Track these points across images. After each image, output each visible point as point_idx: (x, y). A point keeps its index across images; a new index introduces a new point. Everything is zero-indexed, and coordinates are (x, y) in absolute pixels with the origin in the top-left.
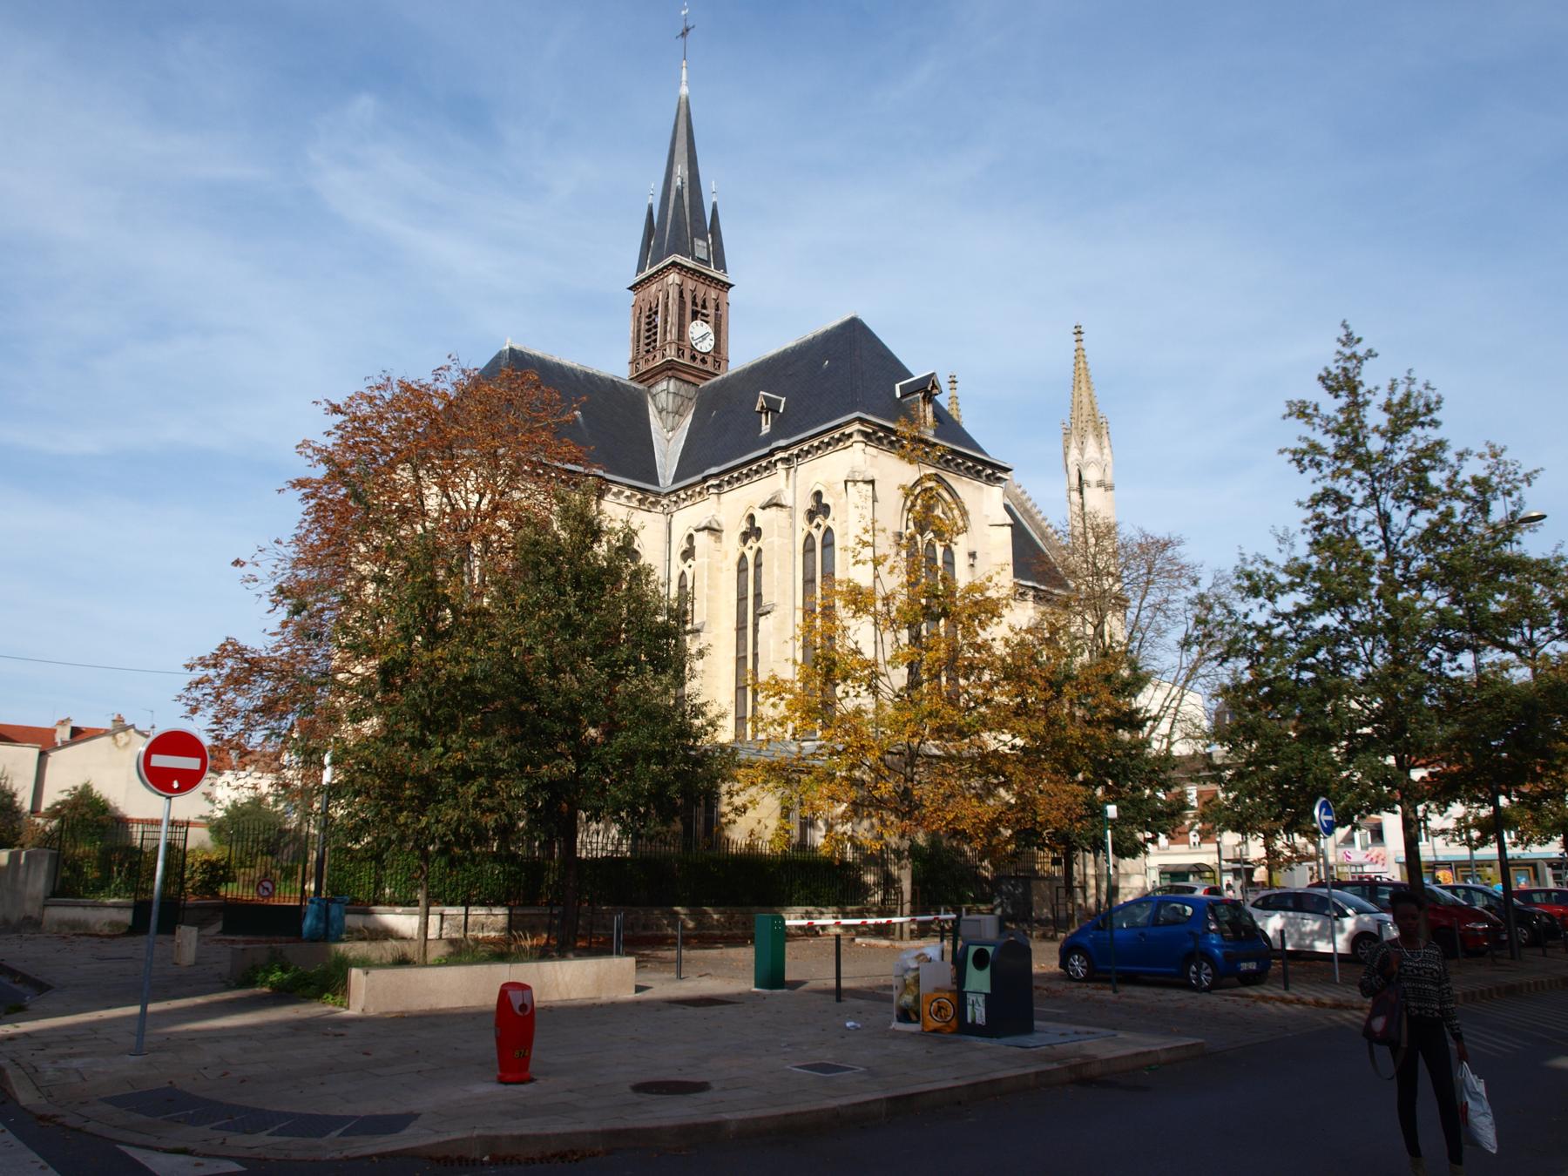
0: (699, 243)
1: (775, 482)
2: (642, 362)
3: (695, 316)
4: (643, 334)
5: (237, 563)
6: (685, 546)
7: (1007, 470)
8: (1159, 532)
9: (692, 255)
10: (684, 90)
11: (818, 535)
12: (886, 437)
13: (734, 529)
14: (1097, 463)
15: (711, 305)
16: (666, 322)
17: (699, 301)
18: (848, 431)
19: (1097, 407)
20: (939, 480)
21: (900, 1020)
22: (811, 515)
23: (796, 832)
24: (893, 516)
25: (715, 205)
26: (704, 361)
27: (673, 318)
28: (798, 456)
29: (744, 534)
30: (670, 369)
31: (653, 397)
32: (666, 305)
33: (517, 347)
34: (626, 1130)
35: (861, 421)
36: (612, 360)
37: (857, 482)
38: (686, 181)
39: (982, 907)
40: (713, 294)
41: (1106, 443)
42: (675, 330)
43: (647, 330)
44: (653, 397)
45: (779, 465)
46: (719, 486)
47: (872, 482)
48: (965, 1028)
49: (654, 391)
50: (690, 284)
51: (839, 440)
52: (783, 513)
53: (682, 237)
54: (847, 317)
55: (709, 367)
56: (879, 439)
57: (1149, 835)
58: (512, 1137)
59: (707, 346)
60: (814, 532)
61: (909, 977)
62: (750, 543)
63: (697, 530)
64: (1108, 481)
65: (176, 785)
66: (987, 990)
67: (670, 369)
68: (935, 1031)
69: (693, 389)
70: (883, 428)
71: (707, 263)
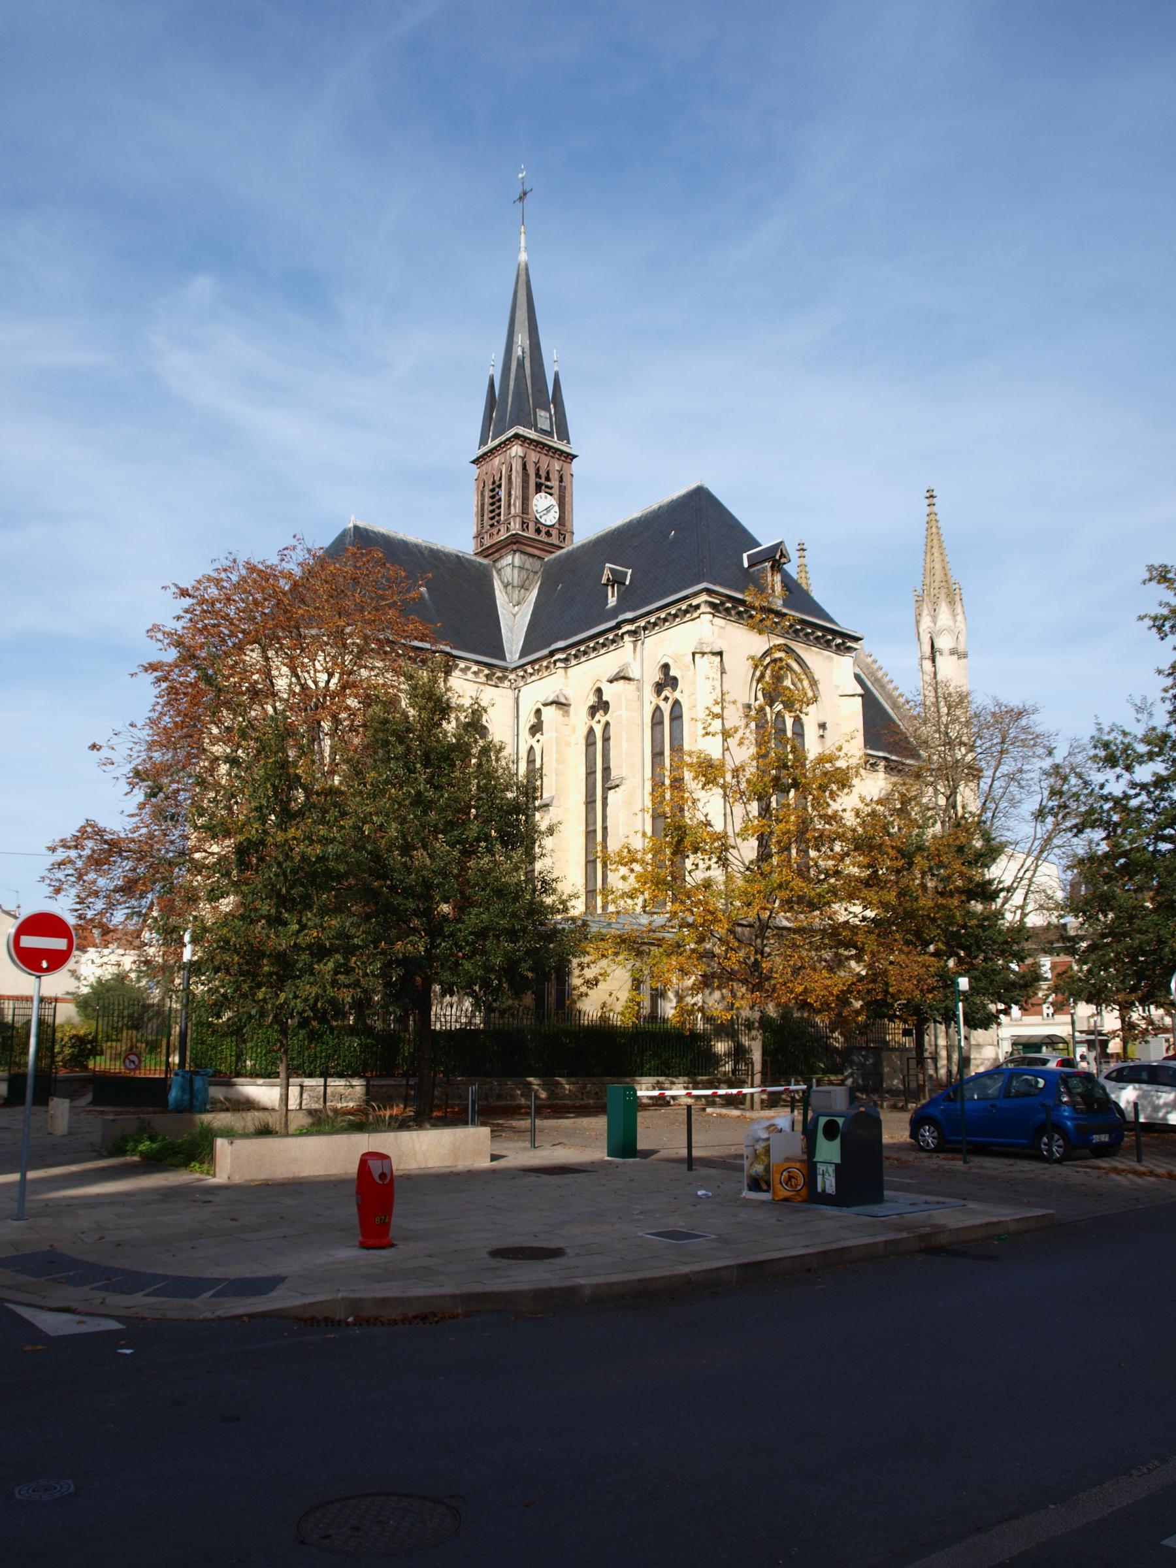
0: (542, 414)
2: (486, 537)
3: (539, 488)
4: (487, 508)
5: (94, 747)
6: (533, 720)
9: (534, 425)
10: (523, 257)
11: (666, 708)
12: (734, 607)
13: (582, 701)
14: (950, 630)
15: (555, 476)
16: (510, 495)
17: (543, 473)
18: (695, 602)
19: (950, 573)
20: (788, 650)
21: (750, 1189)
22: (659, 688)
24: (743, 688)
26: (548, 534)
27: (516, 492)
28: (645, 628)
30: (514, 543)
32: (510, 478)
33: (361, 524)
35: (709, 591)
38: (527, 350)
39: (833, 1078)
41: (959, 610)
42: (519, 503)
45: (626, 638)
46: (566, 660)
47: (720, 654)
50: (533, 456)
52: (631, 687)
53: (525, 408)
54: (692, 486)
55: (554, 540)
56: (727, 610)
58: (375, 1299)
59: (551, 519)
60: (662, 704)
61: (760, 1147)
63: (545, 705)
64: (961, 649)
65: (44, 965)
66: (838, 1160)
67: (514, 543)
68: (786, 1199)
69: (538, 563)
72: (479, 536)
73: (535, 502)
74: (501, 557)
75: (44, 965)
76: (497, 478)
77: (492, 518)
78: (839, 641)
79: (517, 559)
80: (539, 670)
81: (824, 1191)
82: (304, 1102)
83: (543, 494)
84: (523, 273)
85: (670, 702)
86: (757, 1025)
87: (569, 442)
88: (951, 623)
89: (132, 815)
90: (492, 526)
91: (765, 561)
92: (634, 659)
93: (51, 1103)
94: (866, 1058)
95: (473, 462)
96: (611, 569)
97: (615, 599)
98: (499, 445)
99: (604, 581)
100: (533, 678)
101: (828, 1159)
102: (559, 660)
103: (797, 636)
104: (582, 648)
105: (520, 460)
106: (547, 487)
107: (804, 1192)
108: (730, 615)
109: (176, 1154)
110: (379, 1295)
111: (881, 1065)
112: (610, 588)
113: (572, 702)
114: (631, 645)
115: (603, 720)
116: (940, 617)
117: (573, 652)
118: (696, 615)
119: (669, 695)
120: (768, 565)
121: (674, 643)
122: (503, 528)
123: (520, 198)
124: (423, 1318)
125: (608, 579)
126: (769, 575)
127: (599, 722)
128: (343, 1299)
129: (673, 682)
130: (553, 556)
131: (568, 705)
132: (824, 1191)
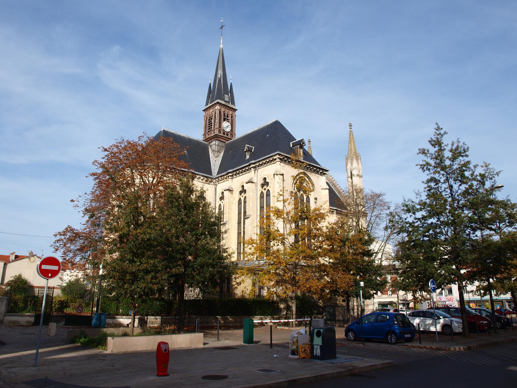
0: (226, 96)
1: (250, 175)
2: (207, 135)
3: (224, 120)
6: (221, 195)
7: (327, 171)
8: (377, 191)
10: (221, 46)
11: (265, 192)
12: (287, 160)
13: (237, 189)
14: (357, 168)
15: (230, 116)
16: (215, 122)
18: (275, 158)
20: (305, 174)
24: (290, 186)
25: (231, 83)
26: (227, 135)
27: (217, 121)
28: (258, 166)
30: (216, 137)
31: (211, 146)
33: (166, 129)
35: (279, 154)
36: (197, 134)
37: (277, 175)
38: (222, 75)
39: (319, 316)
40: (231, 113)
41: (360, 162)
43: (209, 124)
45: (252, 169)
46: (232, 176)
47: (283, 175)
48: (313, 357)
49: (211, 144)
50: (223, 109)
51: (272, 161)
52: (253, 185)
53: (221, 94)
54: (275, 120)
55: (229, 137)
56: (285, 160)
59: (228, 130)
60: (264, 191)
61: (295, 340)
62: (242, 195)
63: (225, 190)
64: (360, 174)
65: (50, 275)
67: (216, 137)
68: (304, 358)
70: (286, 157)
71: (229, 102)
72: (204, 135)
75: (50, 275)
84: (221, 51)
89: (84, 224)
99: (245, 150)
107: (310, 355)
115: (244, 196)
129: (267, 184)
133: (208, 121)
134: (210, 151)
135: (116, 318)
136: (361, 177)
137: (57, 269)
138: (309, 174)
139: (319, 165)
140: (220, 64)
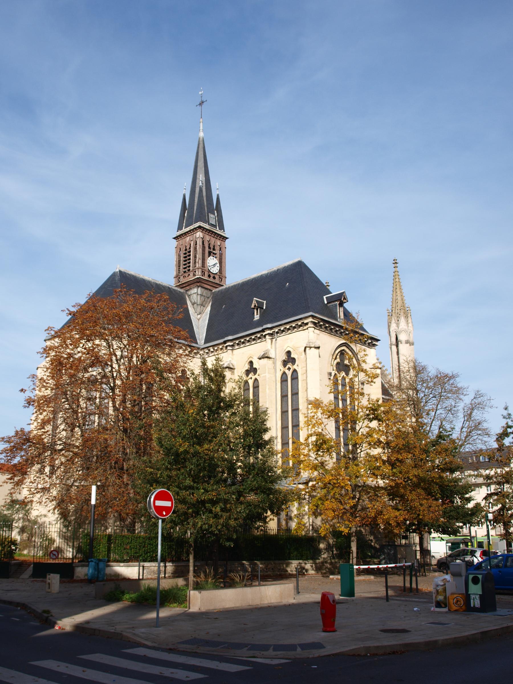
0: (211, 216)
2: (181, 277)
3: (210, 253)
4: (182, 263)
5: (22, 390)
7: (378, 340)
8: (447, 369)
9: (207, 222)
10: (201, 134)
11: (289, 373)
12: (324, 325)
14: (405, 331)
15: (217, 248)
16: (195, 257)
17: (212, 247)
18: (305, 321)
19: (405, 302)
20: (348, 347)
21: (436, 607)
22: (285, 363)
23: (284, 523)
24: (328, 365)
25: (218, 196)
26: (214, 278)
27: (199, 256)
28: (277, 333)
29: (247, 371)
30: (198, 282)
31: (189, 296)
32: (195, 248)
33: (123, 270)
34: (381, 646)
35: (313, 317)
37: (311, 348)
39: (375, 560)
41: (410, 321)
42: (200, 262)
43: (185, 259)
44: (189, 296)
45: (267, 337)
46: (233, 346)
47: (319, 348)
48: (468, 608)
49: (189, 293)
50: (207, 238)
51: (300, 326)
52: (270, 362)
53: (201, 211)
54: (296, 260)
55: (217, 281)
56: (321, 326)
57: (461, 524)
58: (375, 647)
59: (215, 270)
60: (287, 371)
61: (440, 589)
62: (250, 376)
64: (411, 340)
65: (164, 513)
66: (481, 593)
67: (198, 282)
68: (456, 611)
69: (210, 292)
70: (323, 320)
71: (215, 226)
72: (177, 277)
73: (208, 261)
74: (190, 289)
75: (164, 513)
76: (188, 248)
77: (185, 268)
78: (370, 341)
79: (200, 290)
80: (217, 350)
81: (474, 606)
82: (145, 575)
83: (211, 257)
84: (201, 143)
85: (291, 370)
86: (354, 534)
87: (224, 231)
88: (406, 327)
90: (185, 272)
91: (336, 301)
92: (271, 347)
93: (48, 577)
94: (390, 550)
95: (174, 238)
96: (256, 301)
97: (258, 316)
98: (190, 231)
99: (253, 306)
100: (213, 354)
101: (475, 593)
102: (229, 346)
103: (342, 335)
104: (242, 340)
105: (201, 240)
106: (214, 253)
107: (464, 607)
108: (322, 328)
109: (147, 600)
110: (375, 645)
111: (397, 555)
112: (255, 311)
113: (236, 367)
114: (270, 341)
116: (400, 325)
117: (237, 342)
118: (305, 328)
119: (290, 367)
120: (337, 303)
121: (295, 340)
122: (192, 274)
123: (200, 104)
124: (394, 653)
125: (255, 306)
126: (338, 308)
127: (251, 378)
128: (364, 647)
129: (293, 361)
130: (217, 290)
131: (233, 369)
132: (474, 606)
133: (182, 256)
134: (189, 302)
135: (109, 566)
136: (412, 344)
137: (156, 502)
138: (352, 346)
139: (365, 330)
140: (201, 164)
